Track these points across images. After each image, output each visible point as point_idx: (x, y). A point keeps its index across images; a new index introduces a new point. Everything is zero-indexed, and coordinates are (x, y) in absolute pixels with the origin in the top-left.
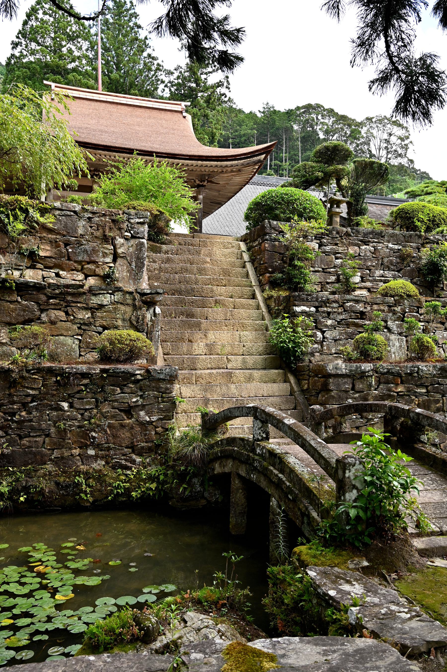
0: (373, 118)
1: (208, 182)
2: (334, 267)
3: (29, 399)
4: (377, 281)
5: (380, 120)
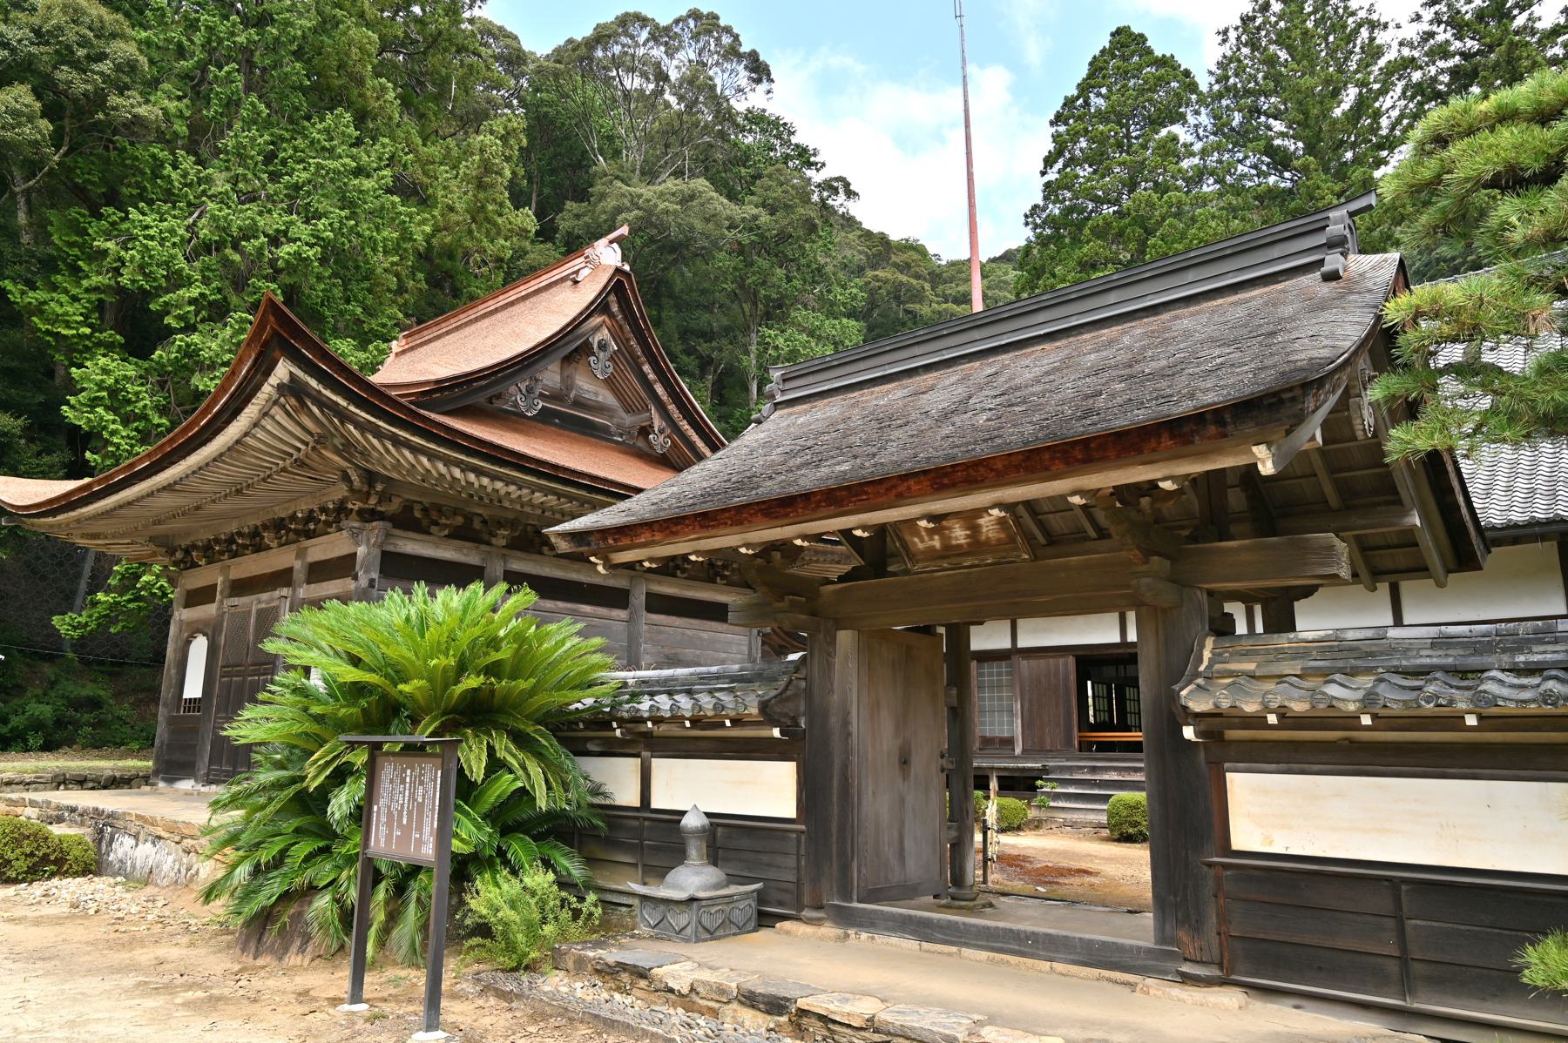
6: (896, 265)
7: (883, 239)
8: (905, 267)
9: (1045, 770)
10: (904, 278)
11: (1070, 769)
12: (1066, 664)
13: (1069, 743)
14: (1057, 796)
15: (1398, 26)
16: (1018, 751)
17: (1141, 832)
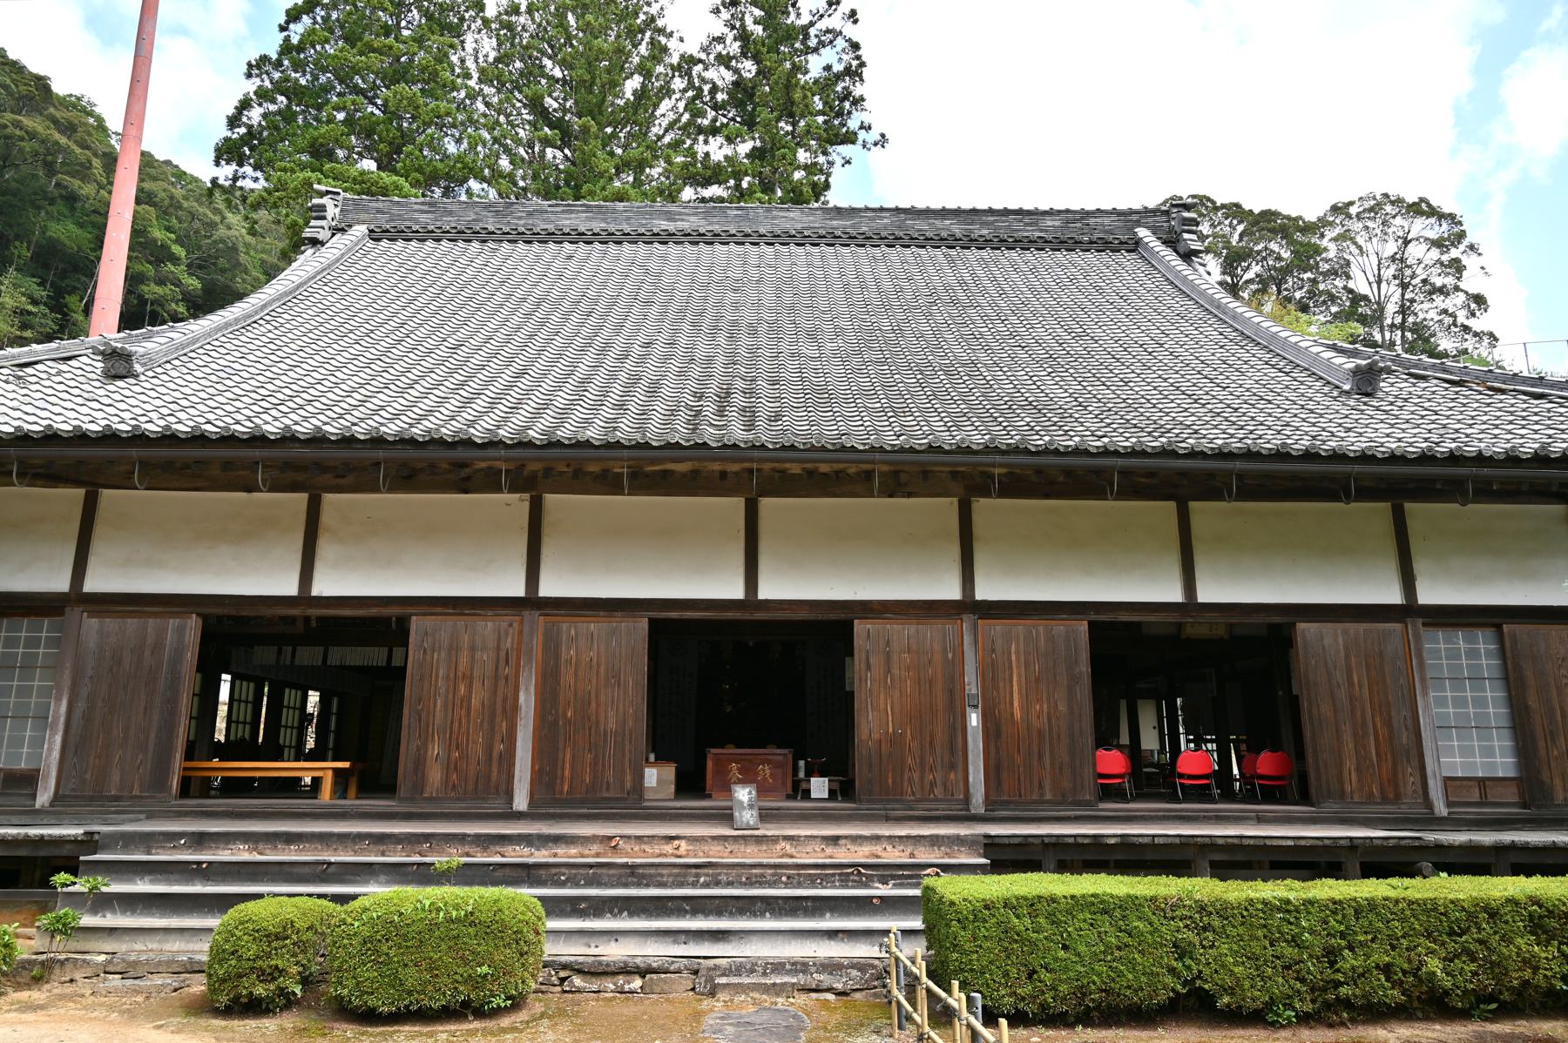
0: (1351, 203)
5: (1371, 209)
6: (55, 121)
7: (42, 83)
8: (69, 129)
9: (90, 843)
10: (63, 140)
11: (147, 841)
12: (181, 631)
13: (158, 780)
14: (103, 902)
15: (682, 40)
16: (43, 798)
17: (282, 991)
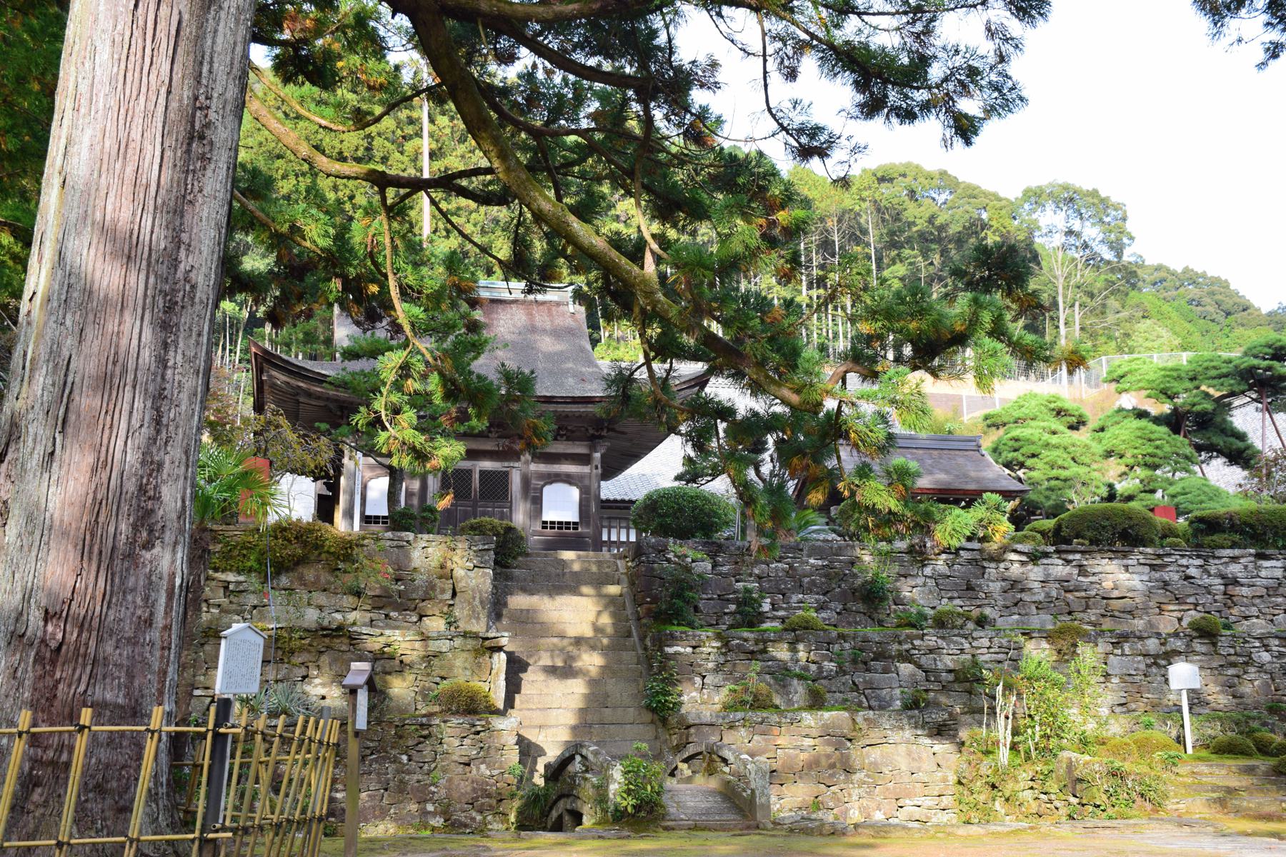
1: (609, 430)
2: (735, 592)
3: (369, 752)
4: (795, 608)
